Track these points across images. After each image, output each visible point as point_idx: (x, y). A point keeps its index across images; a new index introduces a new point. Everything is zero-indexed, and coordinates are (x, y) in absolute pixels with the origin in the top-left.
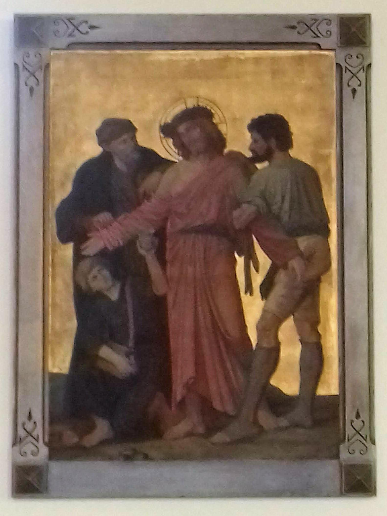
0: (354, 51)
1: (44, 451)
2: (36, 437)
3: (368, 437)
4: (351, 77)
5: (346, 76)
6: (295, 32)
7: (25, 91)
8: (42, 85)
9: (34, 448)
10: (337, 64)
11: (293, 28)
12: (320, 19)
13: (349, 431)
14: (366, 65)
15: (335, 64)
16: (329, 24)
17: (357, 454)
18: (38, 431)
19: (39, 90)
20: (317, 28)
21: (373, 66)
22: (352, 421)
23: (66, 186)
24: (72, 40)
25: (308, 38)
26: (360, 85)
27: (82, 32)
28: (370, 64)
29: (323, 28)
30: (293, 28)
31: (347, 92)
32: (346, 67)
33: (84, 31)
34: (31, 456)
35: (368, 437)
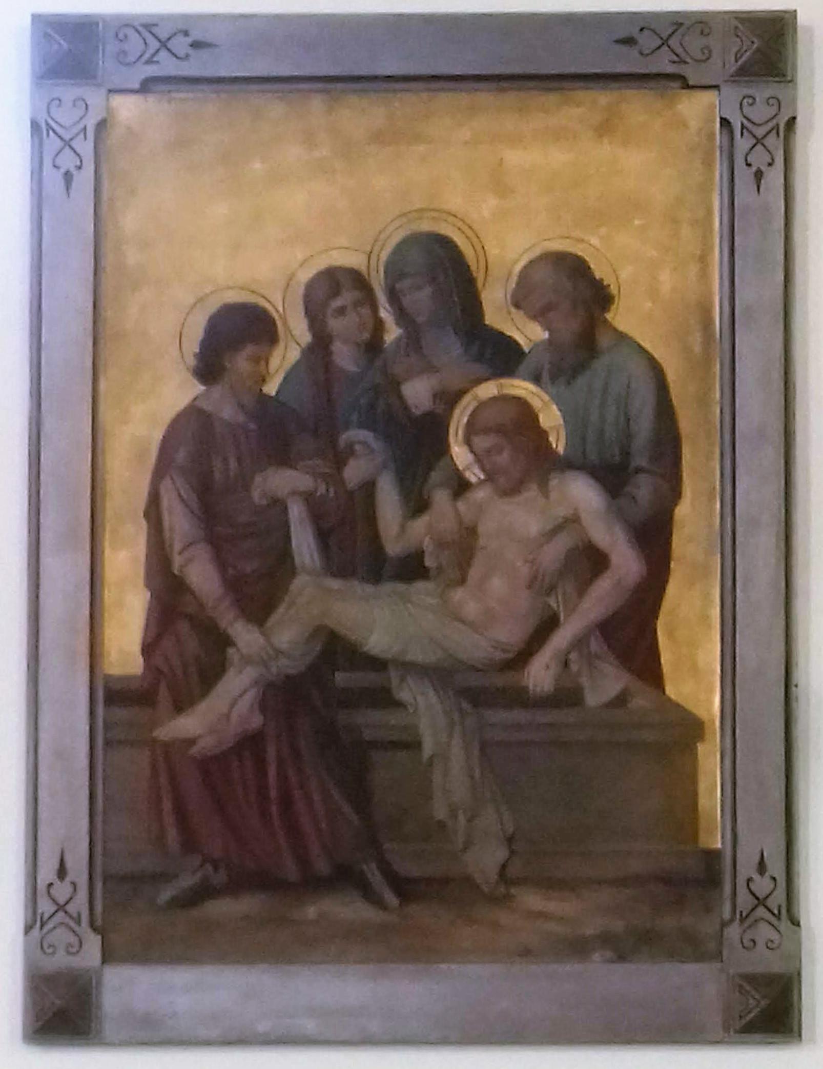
0: (763, 91)
1: (93, 944)
2: (75, 915)
3: (784, 911)
4: (758, 894)
5: (742, 144)
6: (634, 52)
7: (776, 867)
8: (89, 168)
9: (73, 939)
10: (721, 118)
11: (629, 41)
12: (687, 23)
13: (744, 900)
14: (783, 121)
15: (718, 120)
16: (706, 31)
17: (61, 952)
18: (80, 903)
19: (85, 179)
20: (681, 44)
21: (799, 119)
22: (749, 880)
23: (796, 686)
24: (151, 71)
25: (663, 64)
26: (749, 880)
27: (178, 56)
28: (794, 118)
29: (694, 44)
30: (629, 41)
31: (776, 867)
32: (742, 124)
33: (181, 54)
34: (56, 956)
35: (784, 911)
